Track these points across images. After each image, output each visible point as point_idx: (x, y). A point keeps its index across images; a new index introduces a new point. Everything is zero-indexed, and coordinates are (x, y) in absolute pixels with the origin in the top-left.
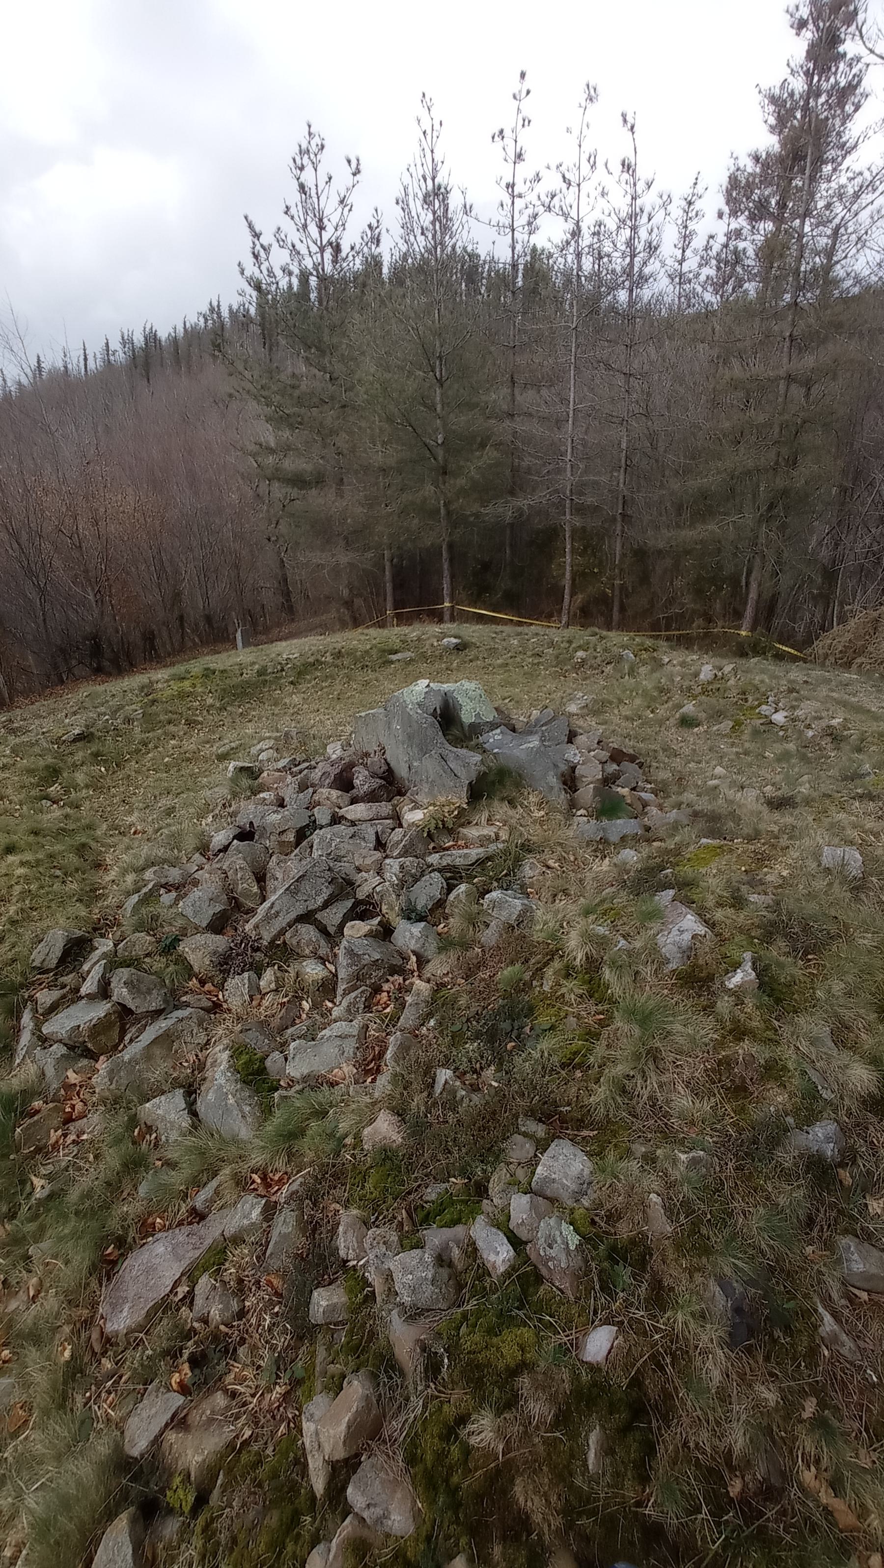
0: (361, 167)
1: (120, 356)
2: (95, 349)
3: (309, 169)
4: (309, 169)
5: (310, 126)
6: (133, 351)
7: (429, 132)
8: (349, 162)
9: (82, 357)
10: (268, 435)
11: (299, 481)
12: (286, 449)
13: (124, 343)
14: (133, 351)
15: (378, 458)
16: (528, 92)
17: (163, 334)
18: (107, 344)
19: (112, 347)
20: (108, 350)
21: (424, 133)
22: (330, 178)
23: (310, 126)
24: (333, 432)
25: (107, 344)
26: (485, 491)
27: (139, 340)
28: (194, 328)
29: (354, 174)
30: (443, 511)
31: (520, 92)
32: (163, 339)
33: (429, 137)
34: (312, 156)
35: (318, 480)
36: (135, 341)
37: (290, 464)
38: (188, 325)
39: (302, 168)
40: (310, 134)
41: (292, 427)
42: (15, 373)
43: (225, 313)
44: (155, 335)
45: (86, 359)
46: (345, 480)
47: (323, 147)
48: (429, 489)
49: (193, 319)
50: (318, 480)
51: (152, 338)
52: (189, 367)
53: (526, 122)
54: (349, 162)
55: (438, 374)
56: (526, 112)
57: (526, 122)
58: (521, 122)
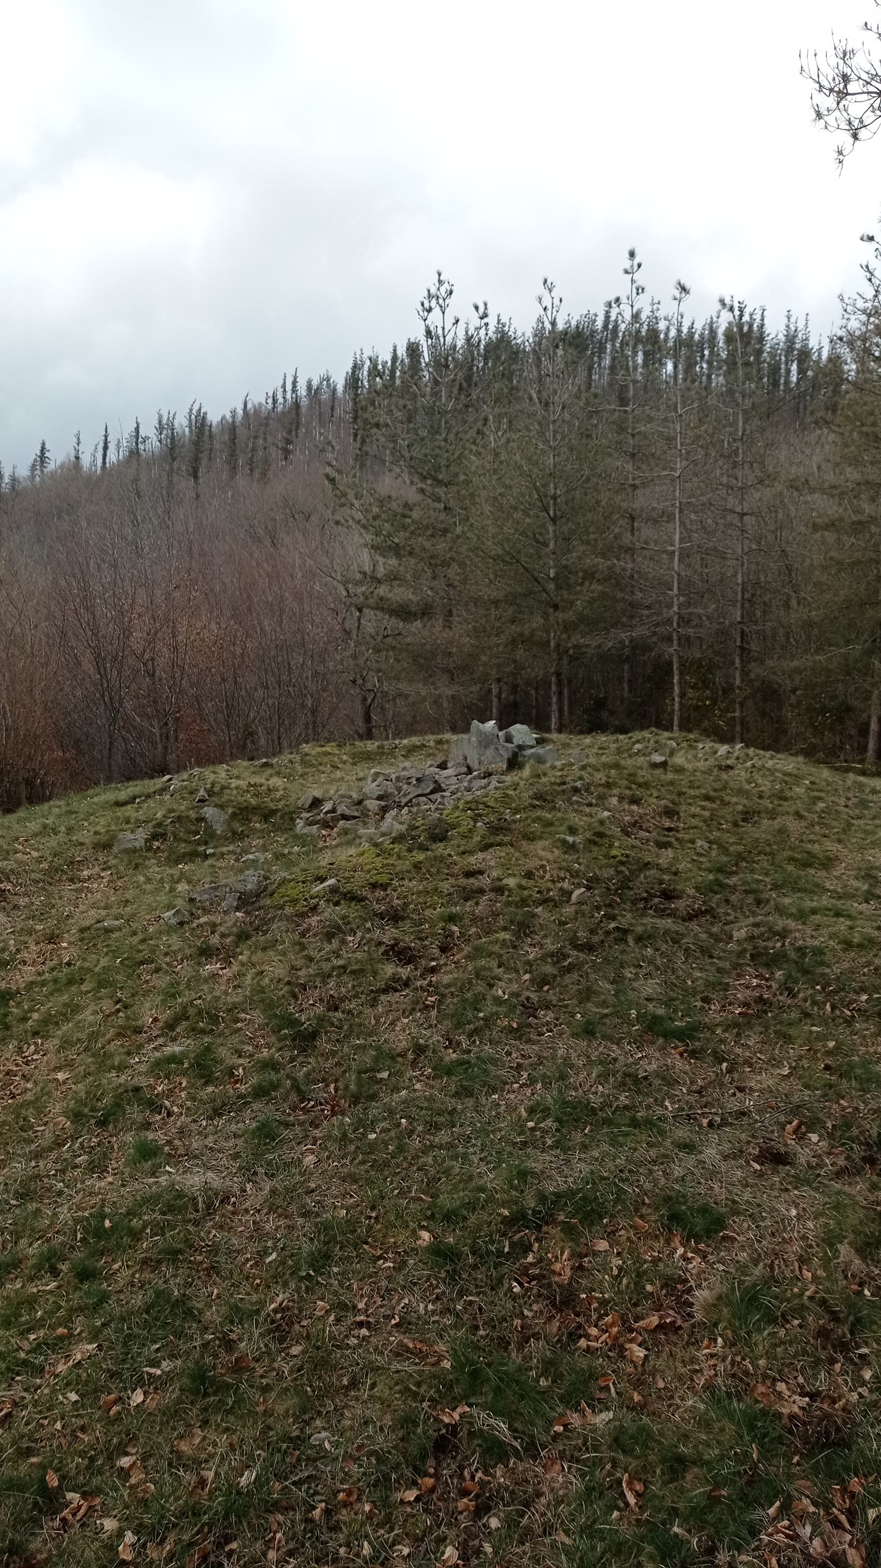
0: (489, 312)
1: (153, 443)
2: (121, 434)
3: (437, 311)
4: (437, 311)
5: (440, 275)
6: (173, 438)
7: (550, 307)
8: (477, 308)
9: (101, 445)
10: (365, 559)
11: (403, 612)
12: (394, 577)
13: (160, 428)
14: (173, 438)
15: (488, 593)
16: (639, 266)
17: (214, 418)
18: (137, 429)
19: (142, 433)
20: (137, 437)
21: (545, 309)
22: (457, 321)
23: (440, 275)
24: (446, 564)
25: (137, 429)
26: (590, 623)
27: (181, 422)
28: (257, 410)
29: (482, 318)
30: (552, 644)
31: (632, 266)
32: (214, 424)
33: (549, 312)
34: (441, 301)
35: (426, 612)
36: (176, 423)
37: (399, 594)
38: (249, 406)
39: (429, 310)
40: (440, 281)
41: (398, 555)
42: (18, 464)
43: (302, 390)
44: (204, 418)
45: (106, 448)
46: (454, 611)
47: (451, 292)
48: (538, 621)
49: (259, 398)
50: (426, 612)
51: (200, 424)
52: (264, 474)
53: (640, 290)
54: (477, 308)
55: (551, 513)
56: (640, 282)
57: (640, 290)
58: (635, 291)
